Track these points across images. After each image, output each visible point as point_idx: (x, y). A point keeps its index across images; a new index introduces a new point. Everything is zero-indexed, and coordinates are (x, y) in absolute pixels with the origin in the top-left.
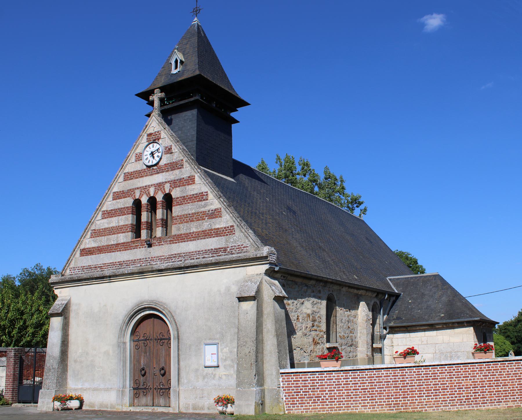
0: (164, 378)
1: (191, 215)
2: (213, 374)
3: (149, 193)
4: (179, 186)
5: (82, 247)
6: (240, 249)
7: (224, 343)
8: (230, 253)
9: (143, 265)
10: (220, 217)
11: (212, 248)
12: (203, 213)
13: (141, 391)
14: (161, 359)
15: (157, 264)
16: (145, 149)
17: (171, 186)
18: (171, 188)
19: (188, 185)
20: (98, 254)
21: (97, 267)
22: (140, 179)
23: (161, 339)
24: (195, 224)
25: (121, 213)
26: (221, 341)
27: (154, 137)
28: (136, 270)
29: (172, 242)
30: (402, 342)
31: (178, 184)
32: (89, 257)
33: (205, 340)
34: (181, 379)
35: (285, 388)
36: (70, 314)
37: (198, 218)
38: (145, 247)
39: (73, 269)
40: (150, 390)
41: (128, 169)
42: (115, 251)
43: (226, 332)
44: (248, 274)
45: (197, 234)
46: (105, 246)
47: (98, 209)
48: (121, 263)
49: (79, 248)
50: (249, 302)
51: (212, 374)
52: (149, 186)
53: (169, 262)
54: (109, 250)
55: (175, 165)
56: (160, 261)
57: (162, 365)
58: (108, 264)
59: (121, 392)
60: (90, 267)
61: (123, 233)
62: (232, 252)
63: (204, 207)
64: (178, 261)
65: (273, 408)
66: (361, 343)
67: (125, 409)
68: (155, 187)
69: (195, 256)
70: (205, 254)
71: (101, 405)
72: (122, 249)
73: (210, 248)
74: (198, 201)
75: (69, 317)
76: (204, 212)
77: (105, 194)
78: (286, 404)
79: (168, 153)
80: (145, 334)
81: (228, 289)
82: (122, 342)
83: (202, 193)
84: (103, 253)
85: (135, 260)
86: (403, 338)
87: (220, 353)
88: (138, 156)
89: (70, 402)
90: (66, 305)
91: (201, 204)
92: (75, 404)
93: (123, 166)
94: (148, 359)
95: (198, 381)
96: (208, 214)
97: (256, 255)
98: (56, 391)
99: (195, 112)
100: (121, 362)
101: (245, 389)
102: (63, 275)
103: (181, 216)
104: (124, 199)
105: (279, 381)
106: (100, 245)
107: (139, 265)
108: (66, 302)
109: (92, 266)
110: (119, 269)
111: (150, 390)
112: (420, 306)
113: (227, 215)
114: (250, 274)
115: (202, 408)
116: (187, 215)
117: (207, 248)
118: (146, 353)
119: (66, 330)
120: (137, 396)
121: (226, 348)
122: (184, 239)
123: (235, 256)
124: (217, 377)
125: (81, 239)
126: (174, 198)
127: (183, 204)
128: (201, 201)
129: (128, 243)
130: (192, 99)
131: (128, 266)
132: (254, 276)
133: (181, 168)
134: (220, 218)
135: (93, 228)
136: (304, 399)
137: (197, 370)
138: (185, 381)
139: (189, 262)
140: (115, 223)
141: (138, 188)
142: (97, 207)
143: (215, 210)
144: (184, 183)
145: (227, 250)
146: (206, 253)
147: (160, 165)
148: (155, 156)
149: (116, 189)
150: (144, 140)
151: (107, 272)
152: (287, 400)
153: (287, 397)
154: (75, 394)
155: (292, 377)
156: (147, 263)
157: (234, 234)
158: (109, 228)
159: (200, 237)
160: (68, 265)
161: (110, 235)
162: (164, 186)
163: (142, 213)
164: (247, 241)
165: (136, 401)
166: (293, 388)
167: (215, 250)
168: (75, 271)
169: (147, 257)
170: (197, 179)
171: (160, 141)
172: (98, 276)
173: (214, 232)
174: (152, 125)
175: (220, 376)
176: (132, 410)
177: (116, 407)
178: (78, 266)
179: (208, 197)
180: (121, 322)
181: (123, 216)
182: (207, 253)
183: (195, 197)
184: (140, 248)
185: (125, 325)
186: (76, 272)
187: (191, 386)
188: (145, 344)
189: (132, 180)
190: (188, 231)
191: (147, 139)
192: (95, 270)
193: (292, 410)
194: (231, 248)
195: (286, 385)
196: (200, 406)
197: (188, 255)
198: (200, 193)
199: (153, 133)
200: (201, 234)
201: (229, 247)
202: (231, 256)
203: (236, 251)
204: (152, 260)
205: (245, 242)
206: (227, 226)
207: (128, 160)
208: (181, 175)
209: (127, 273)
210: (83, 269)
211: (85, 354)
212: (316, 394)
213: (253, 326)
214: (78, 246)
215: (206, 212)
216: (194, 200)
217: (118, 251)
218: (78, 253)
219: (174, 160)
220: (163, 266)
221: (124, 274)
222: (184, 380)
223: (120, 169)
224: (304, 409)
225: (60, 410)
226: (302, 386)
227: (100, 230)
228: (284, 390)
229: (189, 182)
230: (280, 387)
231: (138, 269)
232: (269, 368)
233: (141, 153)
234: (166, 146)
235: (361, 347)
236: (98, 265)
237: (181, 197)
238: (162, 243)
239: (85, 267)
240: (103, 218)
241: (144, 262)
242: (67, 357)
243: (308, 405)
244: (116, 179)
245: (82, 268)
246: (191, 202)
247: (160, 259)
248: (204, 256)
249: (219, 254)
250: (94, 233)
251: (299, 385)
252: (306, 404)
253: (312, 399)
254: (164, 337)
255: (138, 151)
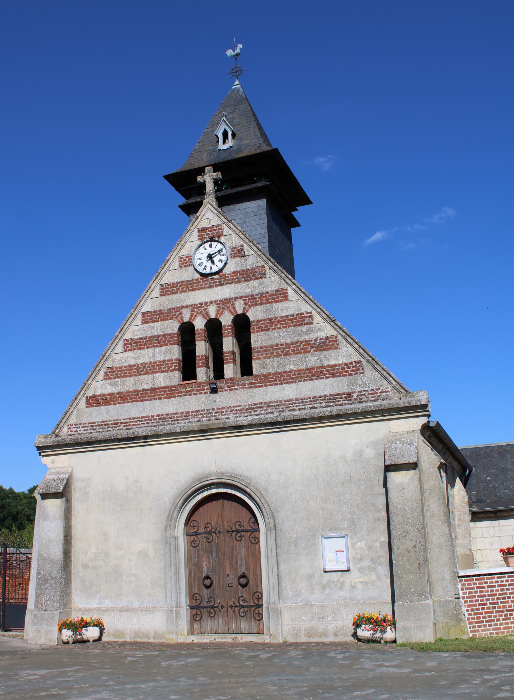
0: (246, 590)
1: (284, 346)
2: (340, 581)
3: (207, 314)
4: (261, 304)
5: (90, 393)
6: (375, 394)
7: (356, 534)
8: (359, 400)
9: (204, 419)
10: (336, 348)
11: (325, 393)
12: (305, 343)
13: (205, 612)
14: (239, 561)
15: (228, 418)
16: (197, 250)
17: (245, 304)
18: (247, 307)
19: (277, 302)
20: (119, 403)
21: (118, 423)
22: (190, 293)
23: (238, 531)
24: (293, 358)
25: (159, 343)
26: (350, 532)
27: (210, 233)
28: (195, 427)
29: (253, 385)
30: (488, 533)
31: (258, 301)
32: (104, 408)
33: (323, 530)
34: (283, 590)
35: (466, 600)
36: (72, 494)
37: (297, 350)
38: (205, 393)
39: (83, 425)
40: (222, 608)
41: (168, 279)
42: (151, 400)
43: (359, 519)
44: (392, 431)
45: (297, 373)
46: (131, 392)
47: (116, 337)
48: (163, 417)
49: (84, 394)
50: (405, 472)
51: (339, 581)
52: (207, 303)
53: (250, 415)
54: (139, 398)
55: (251, 273)
56: (234, 414)
57: (242, 570)
58: (139, 418)
59: (174, 612)
60: (105, 424)
61: (162, 372)
62: (361, 399)
63: (309, 332)
64: (267, 414)
65: (449, 630)
66: (461, 533)
67: (182, 640)
68: (217, 304)
69: (297, 406)
70: (315, 402)
71: (137, 634)
72: (162, 397)
73: (322, 394)
74: (295, 326)
75: (71, 499)
76: (306, 341)
77: (130, 314)
78: (470, 623)
79: (237, 257)
80: (208, 523)
81: (359, 454)
82: (173, 537)
83: (302, 314)
84: (128, 402)
85: (188, 412)
86: (490, 527)
87: (350, 550)
88: (185, 260)
89: (86, 630)
90: (68, 480)
91: (302, 330)
92: (92, 633)
93: (159, 275)
94: (215, 562)
95: (314, 593)
96: (314, 344)
97: (410, 403)
98: (60, 613)
99: (262, 203)
100: (173, 567)
101: (413, 603)
102: (57, 436)
103: (267, 347)
104: (162, 322)
105: (457, 588)
106: (122, 390)
107: (196, 420)
108: (67, 476)
109: (110, 421)
110: (159, 425)
111: (222, 608)
112: (505, 484)
113: (348, 346)
114: (396, 431)
115: (325, 634)
116: (277, 345)
117: (317, 394)
118: (210, 552)
119: (68, 519)
120: (198, 619)
121: (361, 542)
122: (276, 381)
123: (370, 405)
124: (347, 586)
125: (88, 381)
126: (253, 322)
127: (269, 329)
128: (300, 325)
129: (174, 386)
130: (254, 185)
131: (176, 422)
132: (403, 434)
133: (261, 278)
134: (336, 350)
135: (108, 364)
136: (492, 614)
137: (310, 577)
138: (291, 594)
139: (287, 415)
140: (148, 358)
141: (186, 307)
142: (116, 334)
143: (327, 338)
144: (268, 299)
145: (353, 396)
146: (316, 401)
147: (224, 273)
148: (216, 259)
149: (147, 306)
150: (193, 237)
151: (142, 431)
152: (470, 617)
153: (470, 612)
154: (91, 618)
155: (475, 581)
156: (209, 417)
157: (363, 373)
158: (138, 365)
159: (302, 377)
160: (65, 420)
161: (140, 375)
162: (234, 304)
163: (196, 343)
164: (386, 382)
165: (195, 626)
166: (477, 598)
167: (332, 398)
168: (78, 429)
169: (210, 407)
170: (291, 293)
171: (222, 239)
172: (125, 436)
173: (327, 371)
174: (206, 216)
175: (353, 585)
176: (195, 641)
177: (167, 637)
178: (84, 421)
179: (312, 319)
180: (168, 505)
181: (162, 348)
182: (318, 402)
183: (289, 320)
184: (196, 394)
185: (176, 510)
186: (80, 431)
187: (301, 602)
188: (209, 539)
189: (175, 295)
190: (281, 370)
191: (199, 236)
192: (115, 427)
193: (478, 631)
194: (359, 394)
195: (468, 595)
196: (320, 631)
197: (283, 405)
198: (298, 314)
199: (208, 228)
200: (304, 374)
201: (355, 392)
202: (361, 405)
203: (368, 398)
204: (218, 412)
205: (382, 385)
206: (350, 361)
207: (167, 266)
208: (263, 288)
209: (178, 431)
210: (92, 426)
211: (103, 555)
212: (507, 606)
213: (416, 507)
214: (83, 392)
215: (311, 341)
216: (288, 323)
217: (155, 399)
218: (83, 403)
219: (248, 267)
220: (244, 420)
221: (172, 433)
222: (288, 593)
223: (155, 278)
224: (493, 629)
225: (71, 643)
226: (489, 595)
227: (121, 367)
228: (465, 602)
229: (277, 298)
230: (459, 598)
231: (198, 425)
232: (439, 570)
233: (190, 256)
234: (234, 246)
235: (462, 540)
236: (120, 420)
237: (265, 320)
238: (236, 387)
239: (96, 424)
240: (125, 351)
241: (205, 416)
242: (71, 561)
243: (498, 622)
244: (148, 294)
245: (90, 425)
246: (283, 327)
247: (234, 410)
248: (313, 405)
249: (339, 403)
250: (110, 372)
251: (484, 593)
252: (496, 622)
253: (503, 614)
254: (242, 528)
255: (184, 252)
